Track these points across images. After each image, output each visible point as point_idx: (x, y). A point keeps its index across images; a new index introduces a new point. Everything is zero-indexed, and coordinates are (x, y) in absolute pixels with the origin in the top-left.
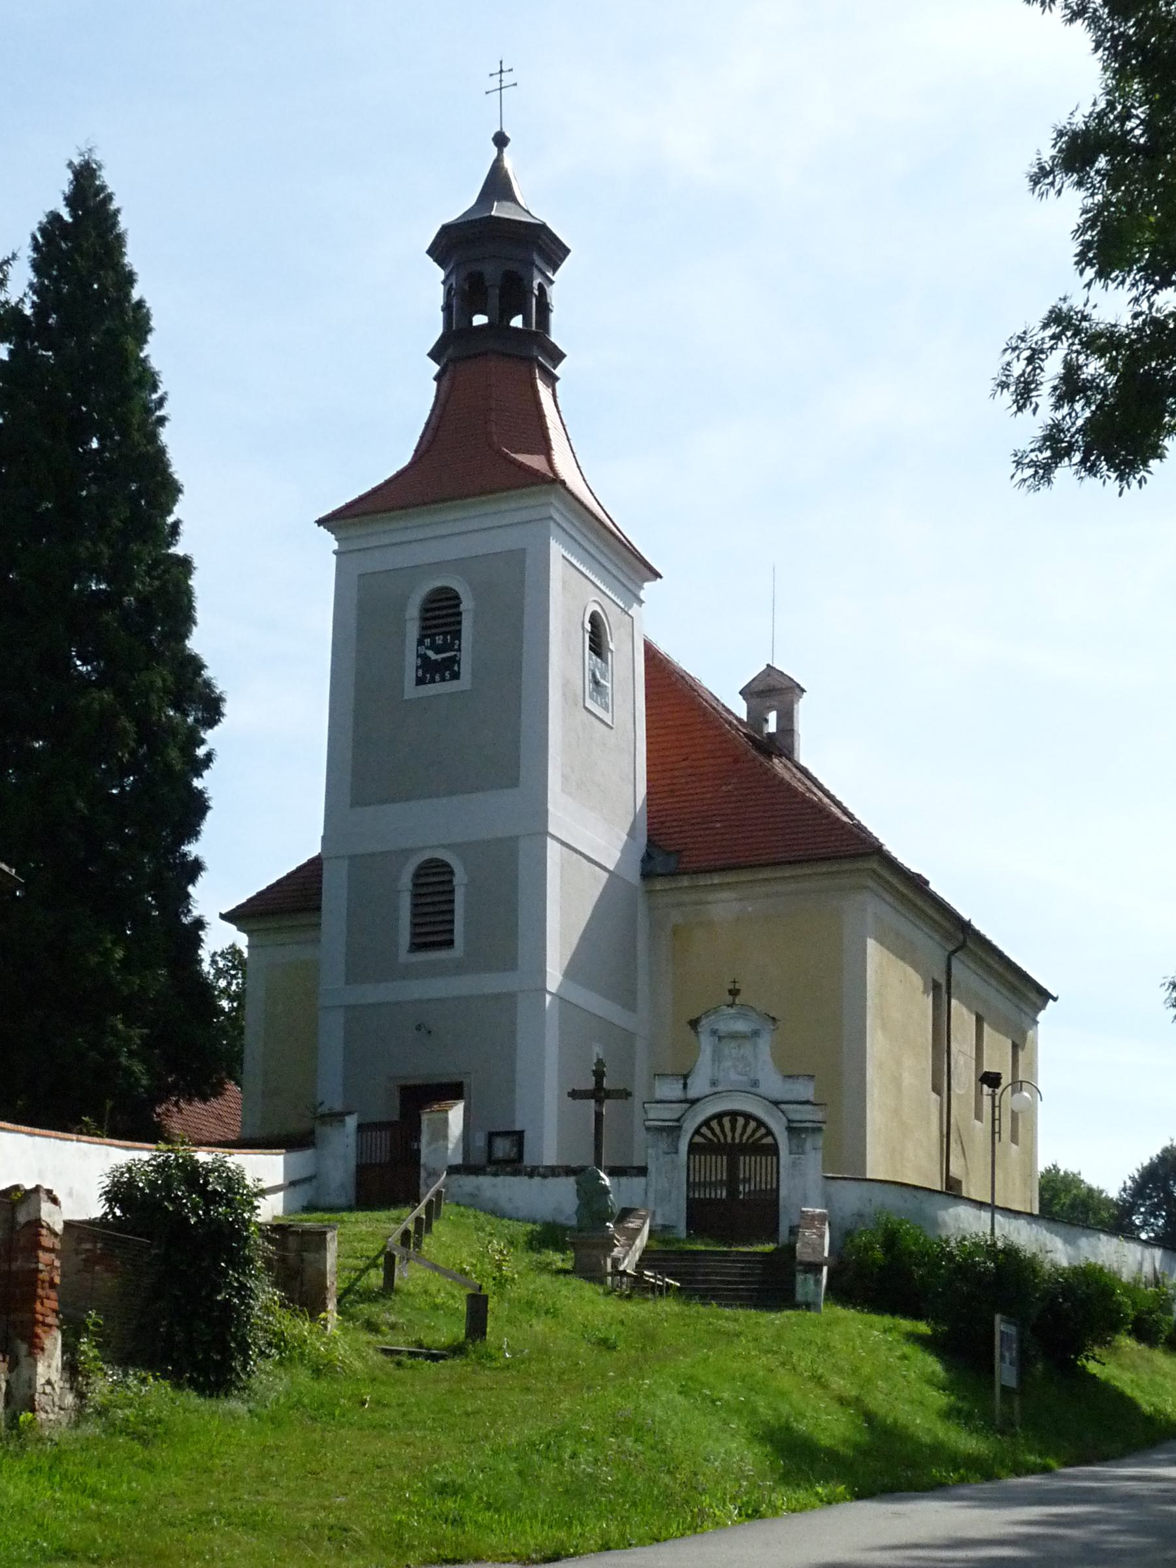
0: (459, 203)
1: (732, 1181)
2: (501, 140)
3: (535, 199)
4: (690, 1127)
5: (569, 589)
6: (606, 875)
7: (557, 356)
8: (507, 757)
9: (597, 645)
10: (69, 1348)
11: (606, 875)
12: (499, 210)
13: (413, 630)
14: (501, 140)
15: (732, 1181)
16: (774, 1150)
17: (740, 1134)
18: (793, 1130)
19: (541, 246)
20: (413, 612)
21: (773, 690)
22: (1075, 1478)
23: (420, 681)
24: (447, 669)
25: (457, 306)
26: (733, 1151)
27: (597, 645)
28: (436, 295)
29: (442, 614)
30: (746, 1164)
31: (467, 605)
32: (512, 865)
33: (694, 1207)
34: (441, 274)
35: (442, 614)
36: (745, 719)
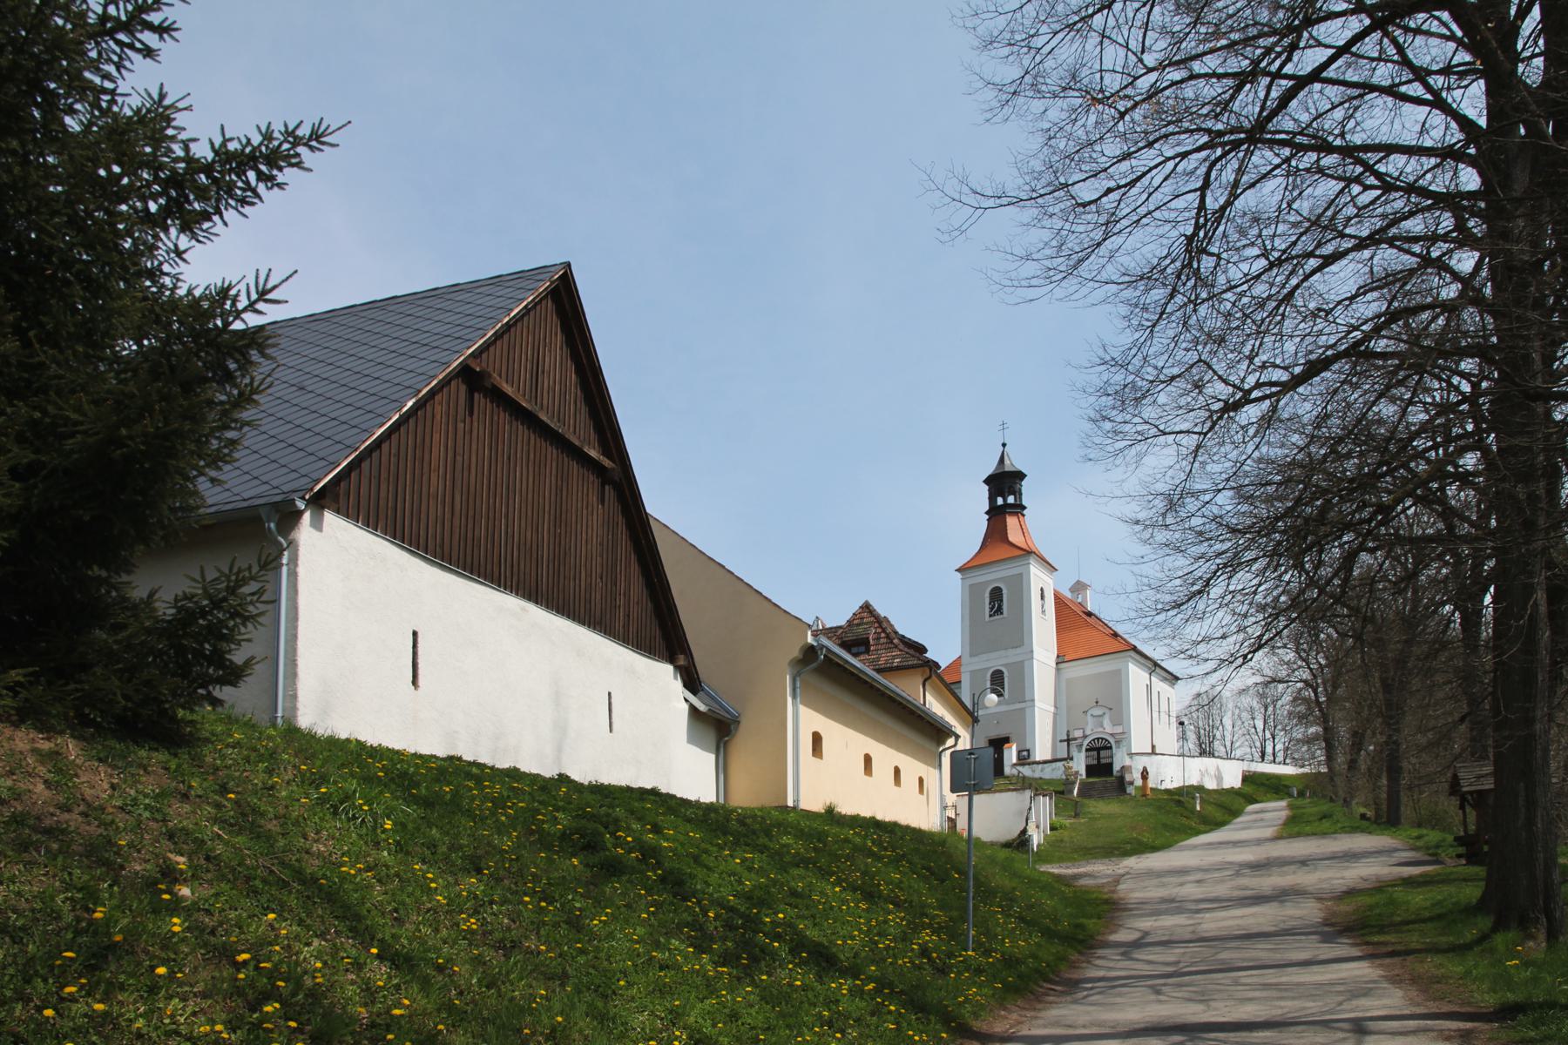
0: (990, 468)
1: (1099, 758)
2: (1004, 445)
3: (1016, 462)
4: (1086, 742)
5: (1037, 577)
6: (976, 798)
7: (1024, 508)
8: (1020, 637)
9: (1042, 597)
10: (1392, 355)
11: (976, 798)
12: (1008, 467)
14: (1004, 445)
15: (1099, 758)
18: (1117, 742)
19: (1020, 476)
21: (1079, 587)
22: (1385, 1007)
24: (999, 611)
25: (992, 499)
26: (1098, 750)
27: (1042, 597)
28: (987, 494)
29: (996, 595)
30: (1103, 753)
31: (1005, 592)
32: (1022, 670)
33: (1088, 767)
35: (996, 595)
36: (1483, 122)
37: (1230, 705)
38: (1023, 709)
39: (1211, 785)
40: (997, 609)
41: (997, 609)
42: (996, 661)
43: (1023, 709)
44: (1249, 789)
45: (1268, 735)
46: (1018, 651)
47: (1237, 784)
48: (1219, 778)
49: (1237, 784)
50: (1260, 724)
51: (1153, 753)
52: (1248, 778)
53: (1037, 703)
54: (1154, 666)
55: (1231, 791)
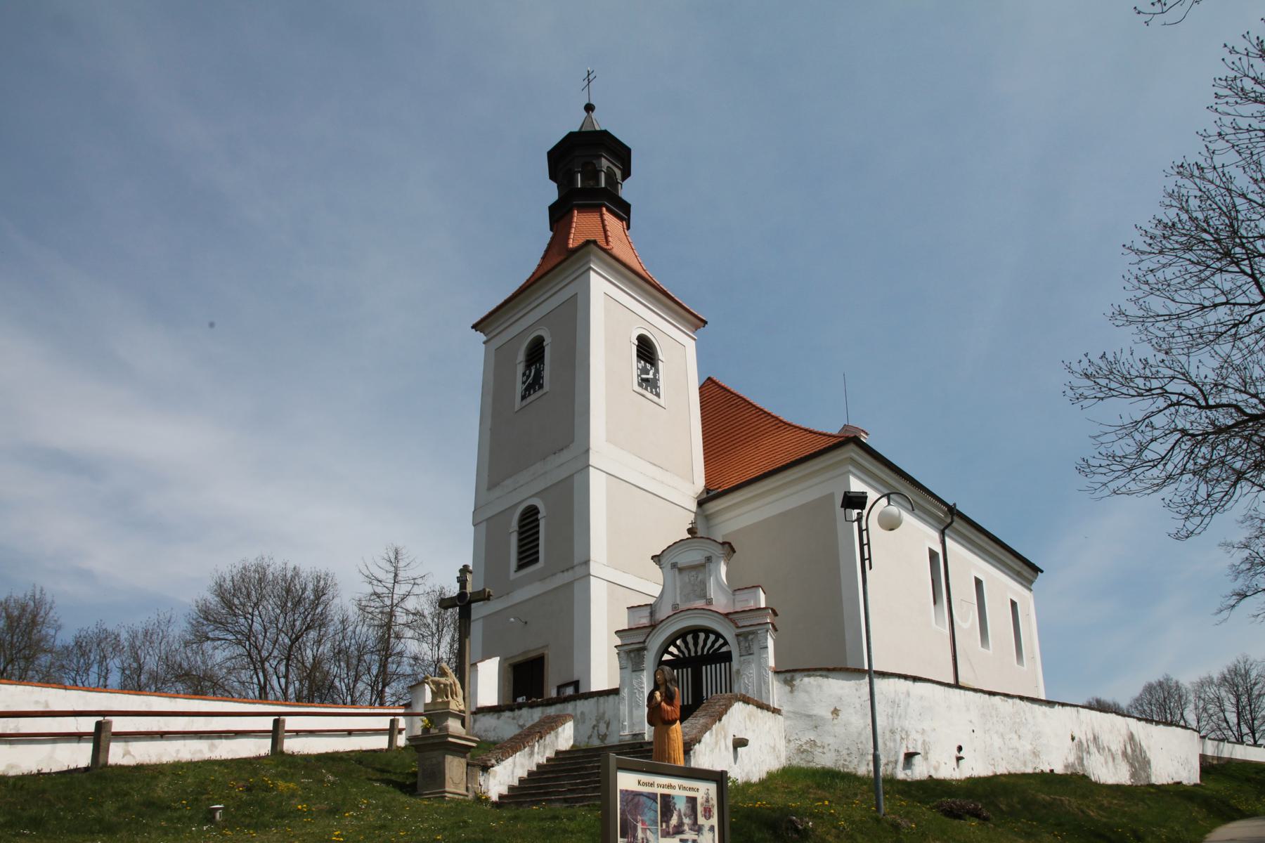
13: (520, 369)
16: (727, 657)
17: (705, 645)
20: (521, 357)
23: (521, 567)
29: (536, 353)
34: (555, 185)
37: (1192, 697)
38: (569, 585)
39: (1109, 771)
40: (534, 384)
41: (534, 384)
42: (524, 490)
43: (569, 585)
44: (1219, 787)
45: (1245, 730)
46: (565, 456)
47: (1190, 775)
48: (1138, 759)
49: (1190, 775)
50: (1232, 718)
51: (957, 685)
52: (1209, 767)
53: (594, 568)
54: (950, 519)
55: (1176, 791)
